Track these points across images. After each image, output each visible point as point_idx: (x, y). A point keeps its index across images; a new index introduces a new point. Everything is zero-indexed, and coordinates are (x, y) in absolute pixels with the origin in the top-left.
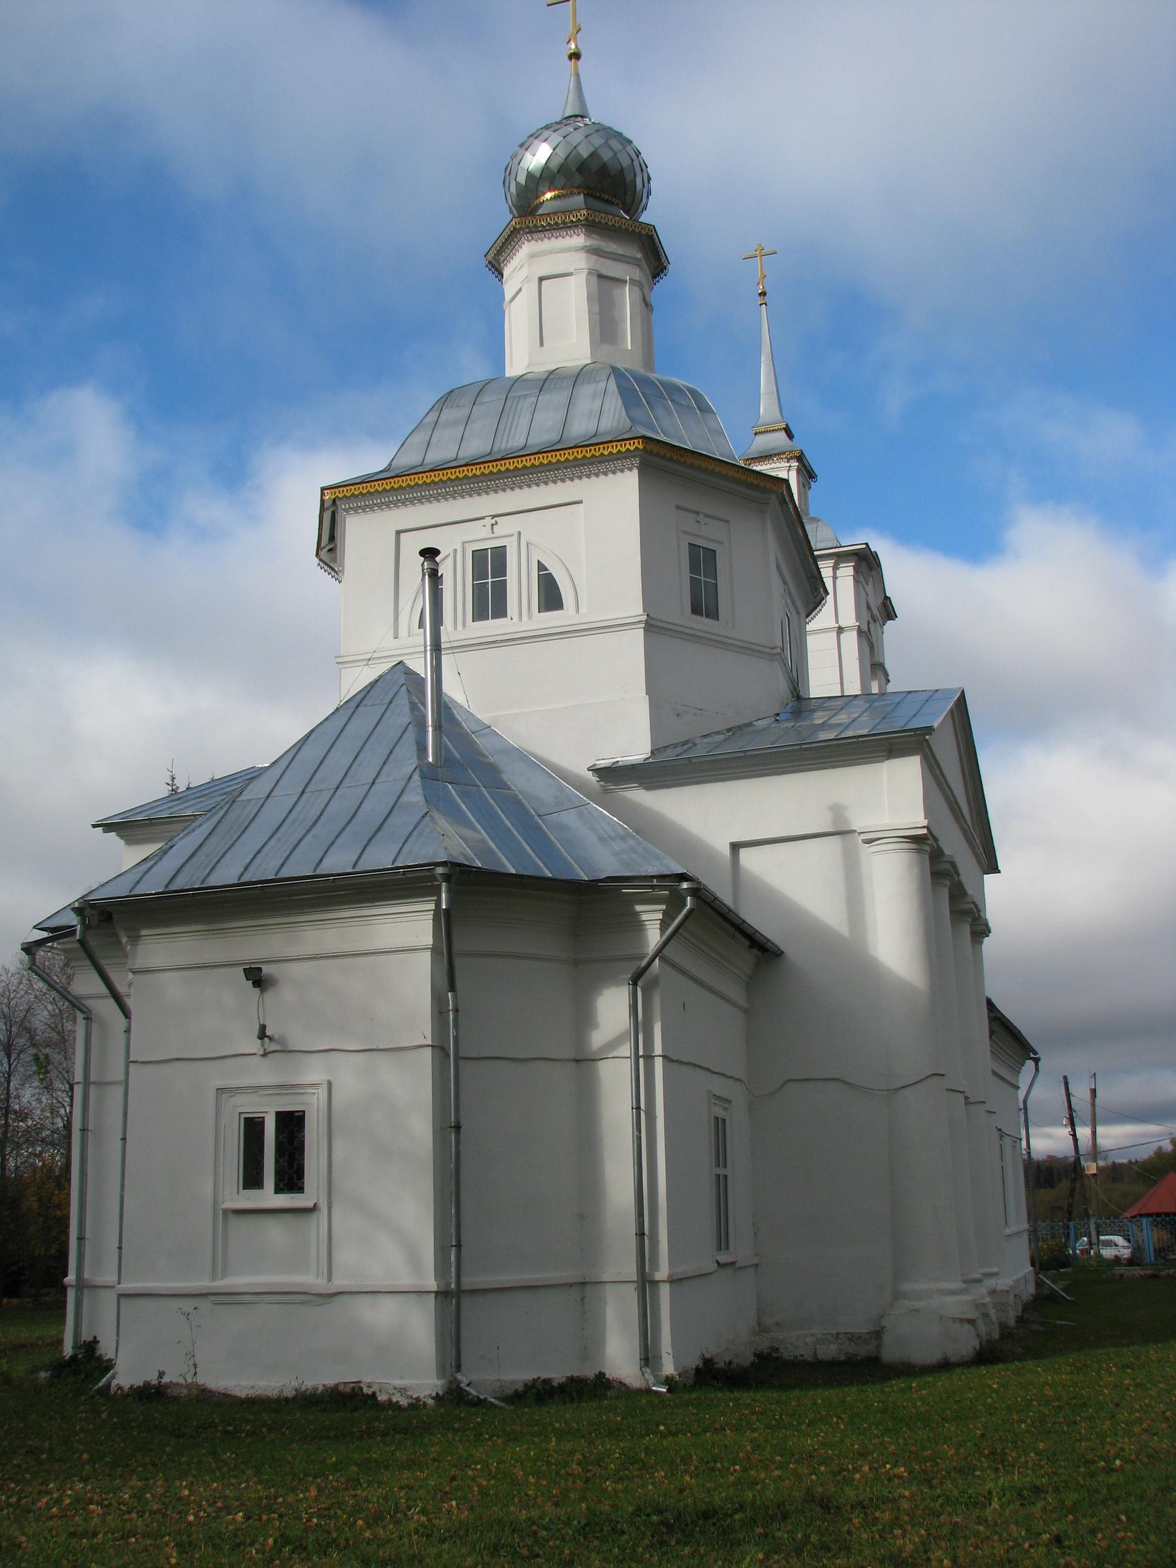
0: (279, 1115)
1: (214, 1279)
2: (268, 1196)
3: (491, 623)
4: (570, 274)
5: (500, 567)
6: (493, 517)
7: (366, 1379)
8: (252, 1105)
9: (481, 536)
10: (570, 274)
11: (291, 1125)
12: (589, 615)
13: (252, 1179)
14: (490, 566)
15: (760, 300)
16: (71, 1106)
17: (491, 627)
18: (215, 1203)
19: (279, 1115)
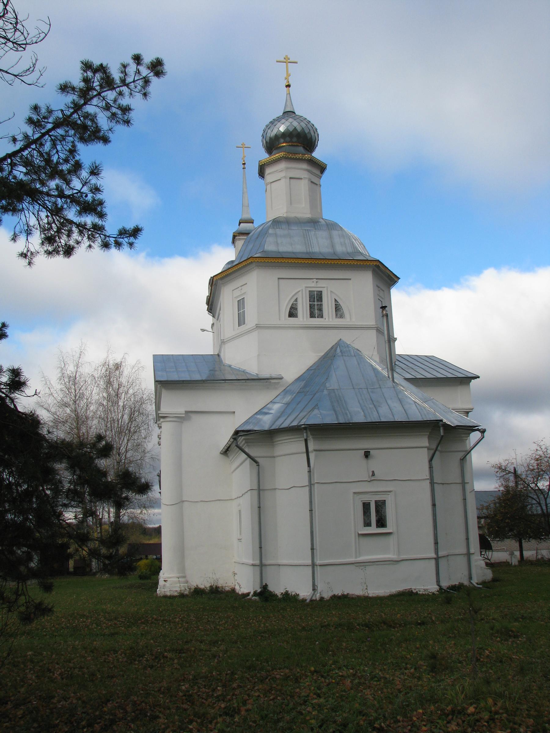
0: (376, 502)
1: (356, 557)
2: (373, 529)
3: (317, 319)
4: (302, 179)
5: (320, 299)
6: (317, 279)
7: (413, 588)
8: (366, 498)
9: (314, 286)
10: (302, 179)
11: (380, 506)
12: (355, 321)
13: (367, 524)
14: (316, 299)
15: (242, 166)
16: (538, 498)
17: (316, 321)
18: (355, 532)
19: (376, 502)
